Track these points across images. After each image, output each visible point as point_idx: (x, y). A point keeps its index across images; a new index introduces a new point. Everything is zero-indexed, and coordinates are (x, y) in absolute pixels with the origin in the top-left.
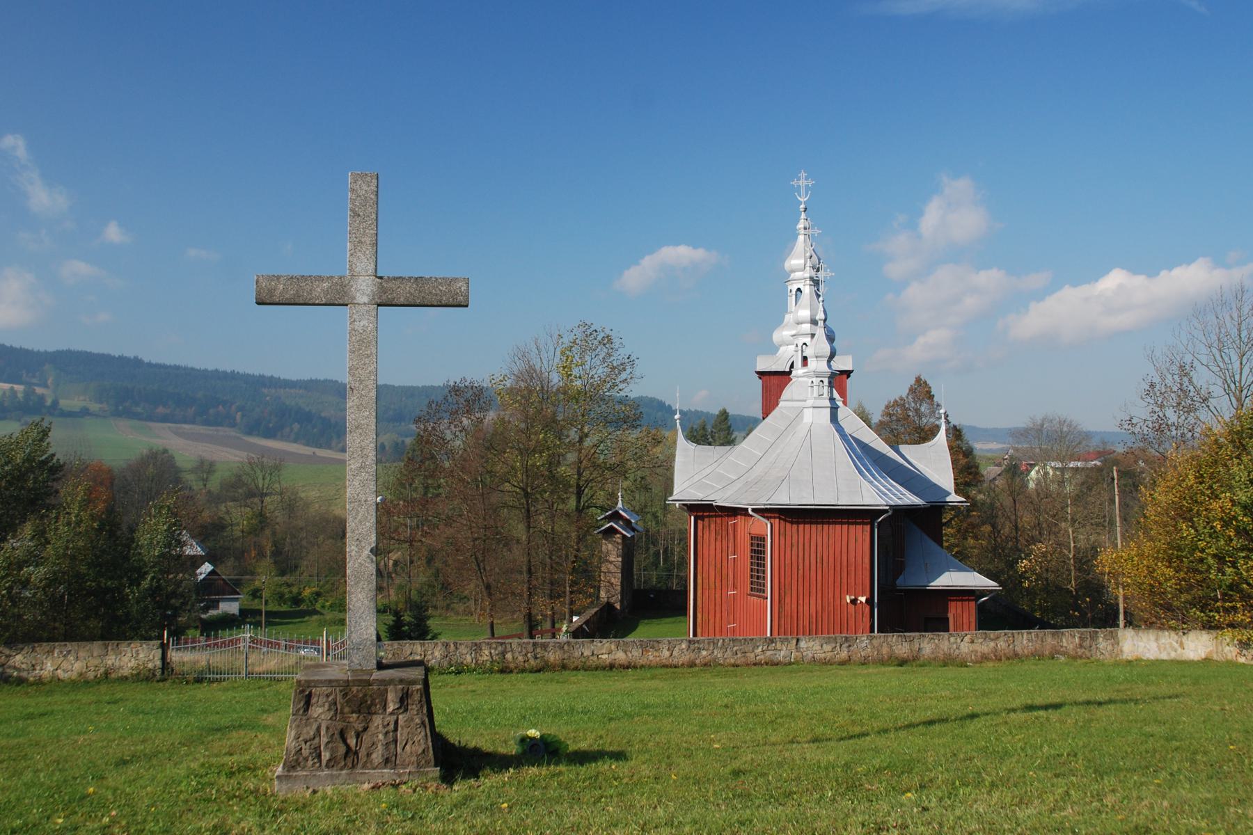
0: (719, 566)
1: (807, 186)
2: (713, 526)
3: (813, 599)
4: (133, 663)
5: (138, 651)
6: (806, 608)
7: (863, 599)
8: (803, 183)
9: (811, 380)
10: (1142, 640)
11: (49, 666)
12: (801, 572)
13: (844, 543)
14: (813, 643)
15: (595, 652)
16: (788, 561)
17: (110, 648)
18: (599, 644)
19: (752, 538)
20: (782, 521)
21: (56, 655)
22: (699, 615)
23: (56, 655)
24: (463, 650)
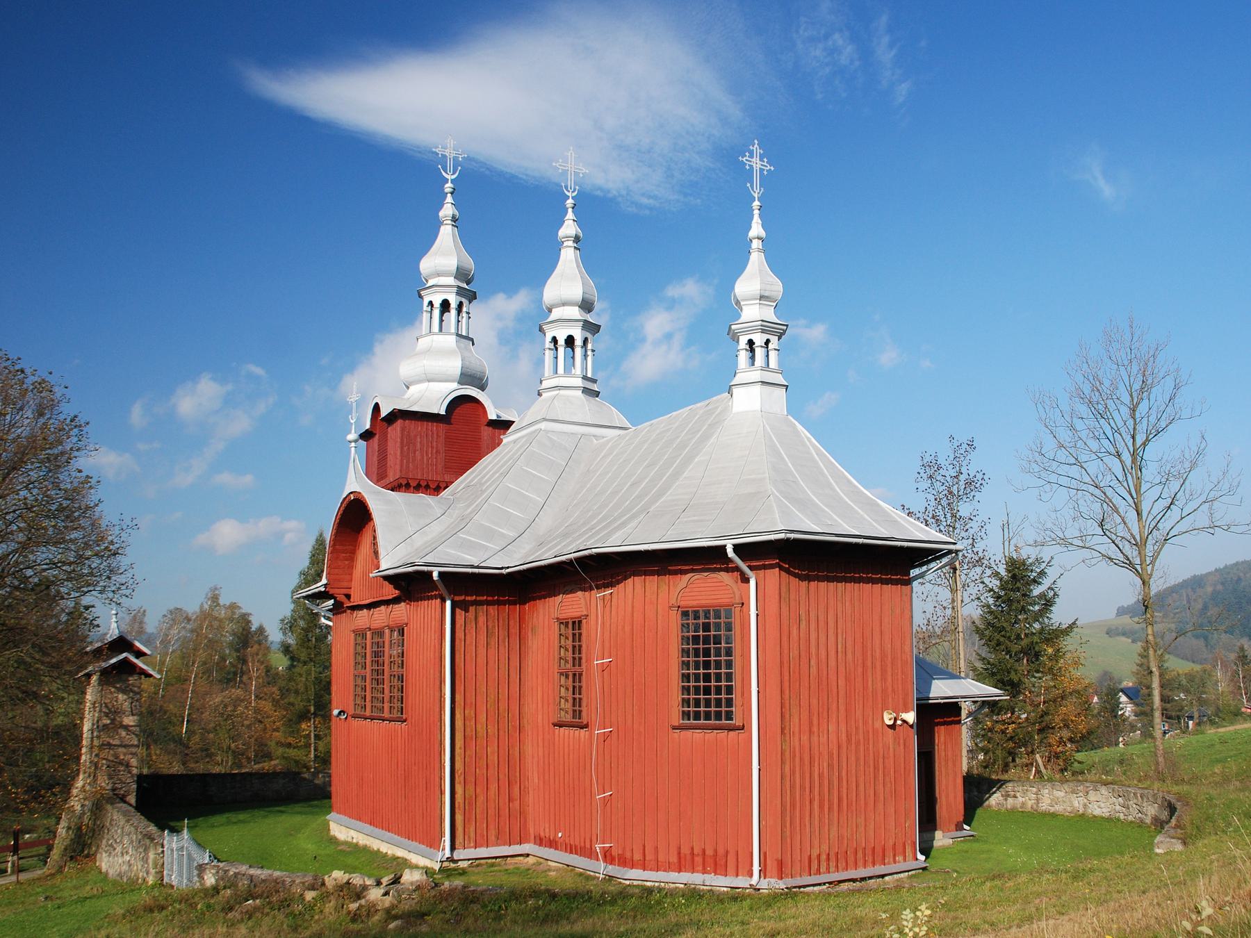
0: (492, 697)
2: (482, 619)
19: (685, 614)
20: (783, 573)
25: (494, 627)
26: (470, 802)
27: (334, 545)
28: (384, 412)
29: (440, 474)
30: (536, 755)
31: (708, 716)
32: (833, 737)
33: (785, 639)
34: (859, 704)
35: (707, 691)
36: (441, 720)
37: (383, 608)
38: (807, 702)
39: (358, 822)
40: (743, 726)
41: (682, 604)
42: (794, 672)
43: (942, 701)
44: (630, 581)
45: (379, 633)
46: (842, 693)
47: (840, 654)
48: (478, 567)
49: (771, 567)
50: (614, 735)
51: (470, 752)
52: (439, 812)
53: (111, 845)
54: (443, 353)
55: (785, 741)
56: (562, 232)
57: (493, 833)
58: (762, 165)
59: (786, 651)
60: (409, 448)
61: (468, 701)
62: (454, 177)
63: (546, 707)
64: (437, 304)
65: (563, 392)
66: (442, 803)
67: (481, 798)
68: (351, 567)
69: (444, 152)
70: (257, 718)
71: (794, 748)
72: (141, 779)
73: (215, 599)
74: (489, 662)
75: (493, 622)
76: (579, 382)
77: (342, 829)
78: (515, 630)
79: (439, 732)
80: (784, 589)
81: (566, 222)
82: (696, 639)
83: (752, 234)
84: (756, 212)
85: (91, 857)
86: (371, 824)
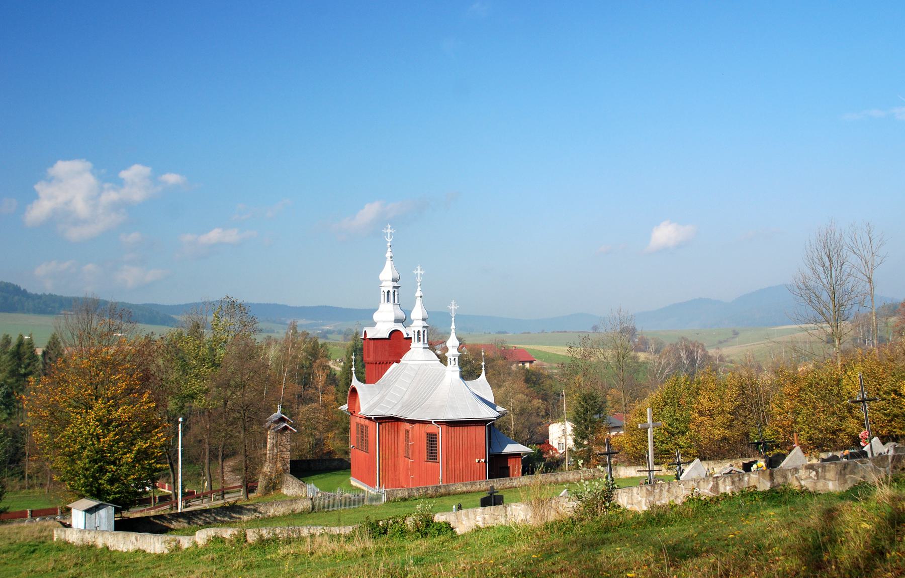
0: (390, 448)
1: (391, 233)
2: (387, 427)
3: (461, 461)
4: (302, 507)
6: (458, 466)
7: (483, 460)
8: (389, 231)
9: (454, 358)
10: (628, 470)
11: (272, 511)
12: (455, 449)
16: (450, 445)
19: (427, 434)
22: (381, 473)
24: (414, 491)
26: (384, 477)
28: (368, 337)
31: (434, 459)
32: (461, 465)
33: (447, 442)
41: (427, 431)
45: (362, 426)
46: (464, 454)
53: (288, 486)
56: (416, 295)
57: (390, 485)
62: (391, 240)
77: (354, 482)
78: (396, 430)
84: (453, 321)
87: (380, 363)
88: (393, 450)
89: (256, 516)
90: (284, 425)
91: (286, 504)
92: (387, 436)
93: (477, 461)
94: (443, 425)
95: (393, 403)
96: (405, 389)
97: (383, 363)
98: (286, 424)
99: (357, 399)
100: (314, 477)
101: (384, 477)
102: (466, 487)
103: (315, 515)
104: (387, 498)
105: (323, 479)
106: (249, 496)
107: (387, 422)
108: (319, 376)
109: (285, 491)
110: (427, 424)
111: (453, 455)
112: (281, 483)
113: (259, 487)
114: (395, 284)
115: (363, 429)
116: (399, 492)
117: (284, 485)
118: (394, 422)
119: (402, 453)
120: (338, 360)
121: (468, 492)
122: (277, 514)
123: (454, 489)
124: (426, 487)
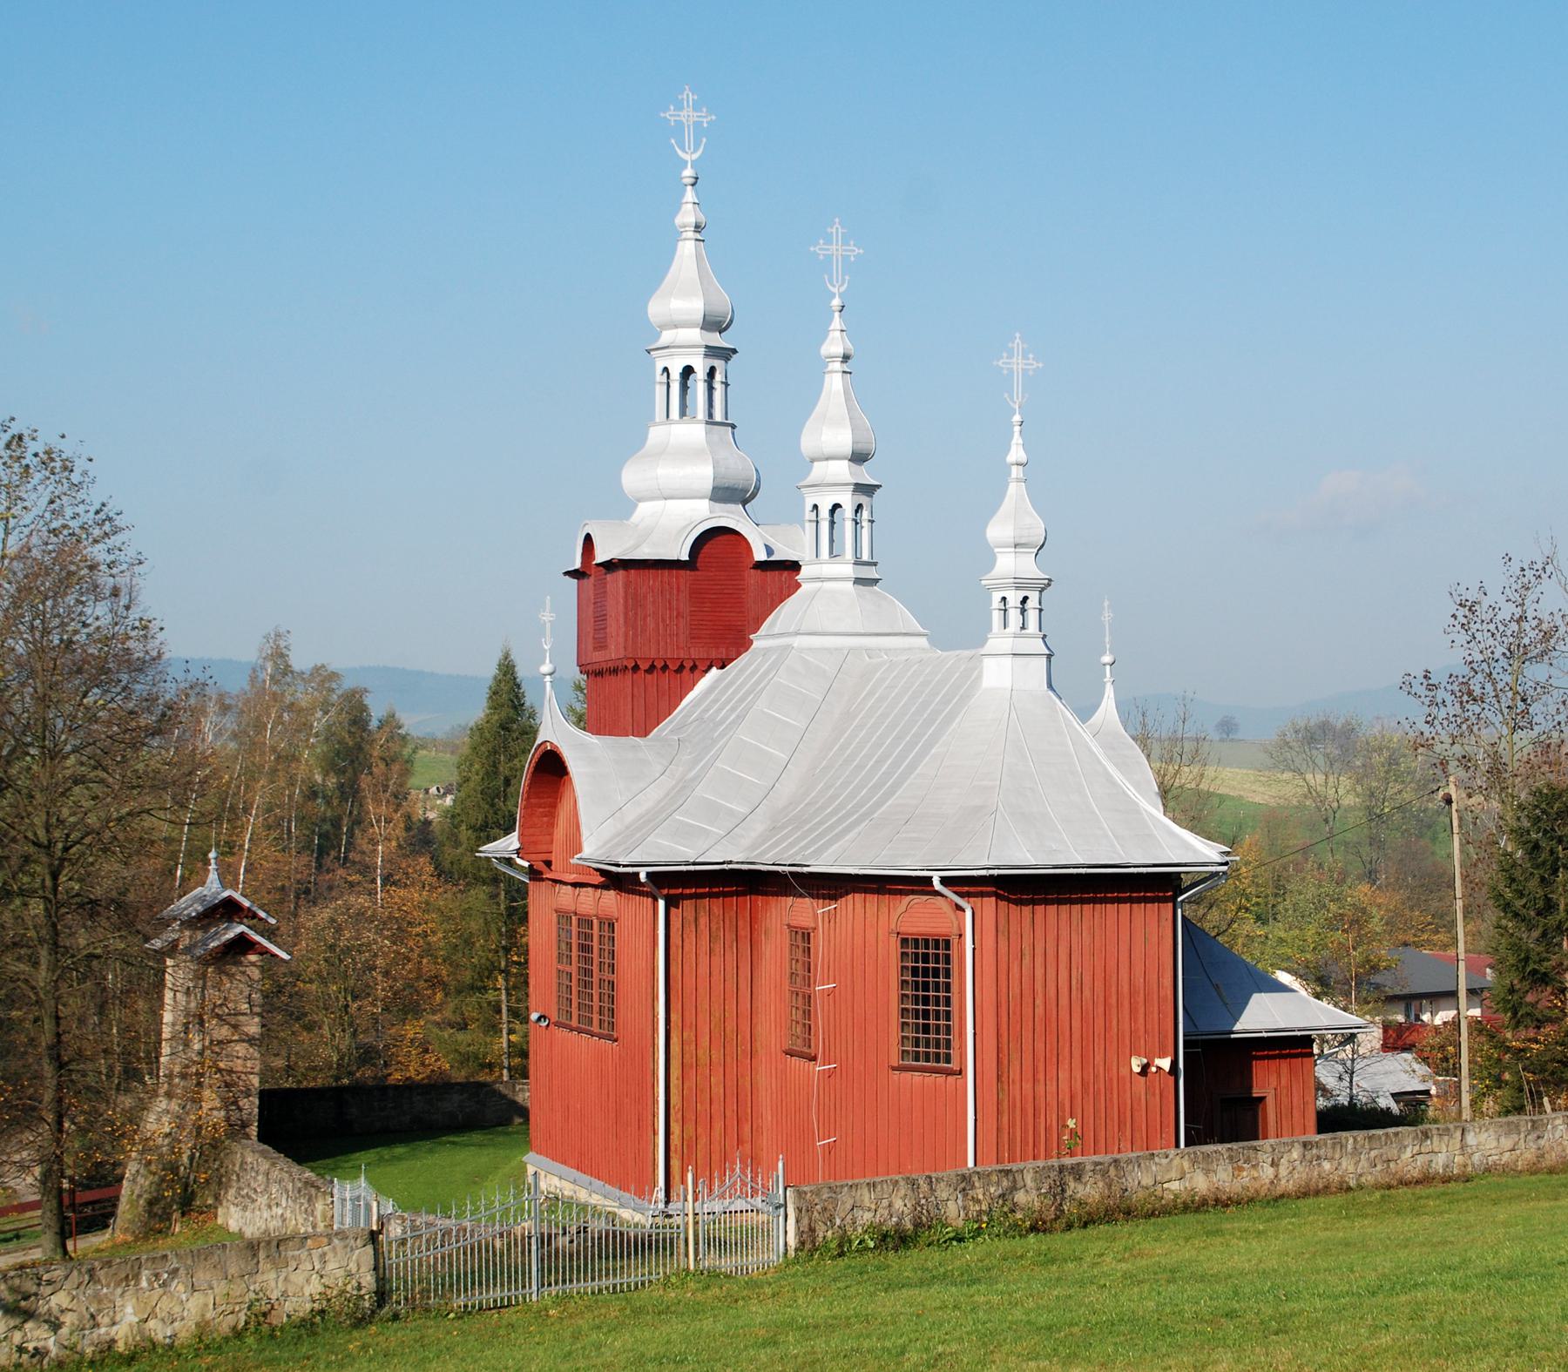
0: (717, 1014)
1: (698, 125)
2: (703, 920)
4: (315, 1287)
5: (324, 1254)
7: (1165, 1064)
8: (688, 116)
9: (1022, 594)
11: (129, 1314)
13: (1124, 948)
14: (1486, 1134)
15: (1159, 1178)
16: (1015, 990)
17: (262, 1255)
18: (1165, 1161)
19: (904, 942)
21: (144, 1284)
23: (144, 1284)
24: (943, 1192)
25: (718, 929)
26: (690, 1145)
27: (528, 798)
28: (601, 556)
29: (683, 648)
30: (769, 1087)
31: (927, 1058)
32: (1064, 1086)
33: (1003, 977)
34: (1099, 1044)
35: (926, 1029)
36: (654, 1044)
37: (590, 889)
38: (1031, 1048)
39: (563, 1166)
40: (961, 1069)
41: (902, 930)
42: (1014, 1013)
43: (1299, 1033)
44: (850, 896)
45: (585, 922)
47: (1074, 993)
48: (694, 864)
49: (989, 895)
50: (838, 1070)
51: (690, 1083)
52: (651, 1155)
54: (687, 454)
55: (1003, 1089)
58: (1026, 364)
59: (1004, 990)
60: (636, 614)
61: (687, 1022)
62: (695, 156)
63: (778, 1030)
64: (676, 375)
65: (827, 585)
66: (655, 1146)
67: (703, 1141)
68: (552, 825)
69: (679, 116)
70: (399, 953)
71: (1014, 1098)
72: (264, 1095)
73: (279, 655)
74: (714, 973)
75: (717, 923)
76: (848, 570)
78: (744, 932)
79: (651, 1059)
80: (1002, 922)
81: (831, 335)
82: (915, 971)
83: (1011, 458)
85: (210, 1211)
86: (578, 1169)
87: (652, 668)
88: (731, 1026)
89: (21, 1349)
90: (230, 935)
91: (220, 1267)
92: (703, 959)
93: (1136, 1065)
94: (982, 895)
95: (731, 812)
96: (785, 757)
97: (665, 667)
98: (241, 928)
99: (566, 795)
100: (363, 1158)
101: (690, 1145)
102: (1207, 1172)
103: (395, 1336)
104: (800, 1233)
105: (405, 1165)
106: (70, 1245)
107: (702, 896)
108: (378, 821)
109: (234, 1218)
110: (907, 893)
111: (1027, 1035)
112: (219, 1183)
113: (123, 1206)
114: (716, 340)
115: (589, 937)
116: (867, 1197)
117: (232, 1192)
118: (737, 894)
119: (772, 1031)
120: (433, 790)
121: (1221, 1203)
122: (159, 1331)
123: (1147, 1181)
124: (1007, 1172)
